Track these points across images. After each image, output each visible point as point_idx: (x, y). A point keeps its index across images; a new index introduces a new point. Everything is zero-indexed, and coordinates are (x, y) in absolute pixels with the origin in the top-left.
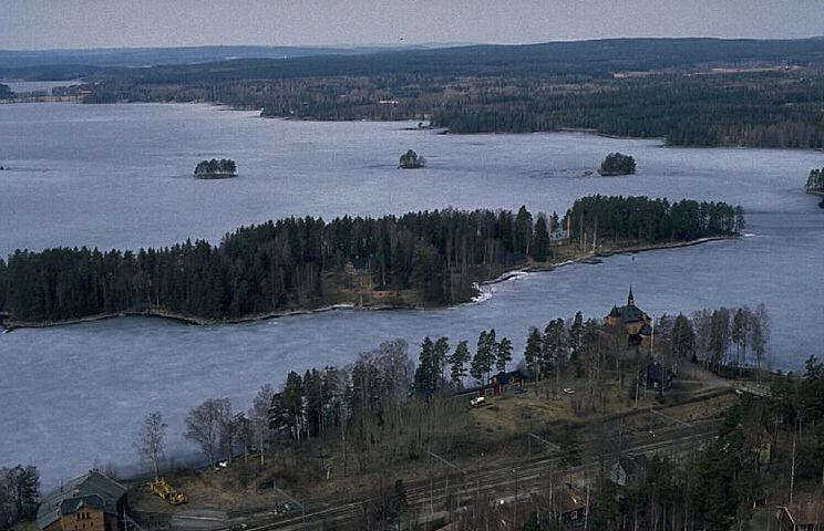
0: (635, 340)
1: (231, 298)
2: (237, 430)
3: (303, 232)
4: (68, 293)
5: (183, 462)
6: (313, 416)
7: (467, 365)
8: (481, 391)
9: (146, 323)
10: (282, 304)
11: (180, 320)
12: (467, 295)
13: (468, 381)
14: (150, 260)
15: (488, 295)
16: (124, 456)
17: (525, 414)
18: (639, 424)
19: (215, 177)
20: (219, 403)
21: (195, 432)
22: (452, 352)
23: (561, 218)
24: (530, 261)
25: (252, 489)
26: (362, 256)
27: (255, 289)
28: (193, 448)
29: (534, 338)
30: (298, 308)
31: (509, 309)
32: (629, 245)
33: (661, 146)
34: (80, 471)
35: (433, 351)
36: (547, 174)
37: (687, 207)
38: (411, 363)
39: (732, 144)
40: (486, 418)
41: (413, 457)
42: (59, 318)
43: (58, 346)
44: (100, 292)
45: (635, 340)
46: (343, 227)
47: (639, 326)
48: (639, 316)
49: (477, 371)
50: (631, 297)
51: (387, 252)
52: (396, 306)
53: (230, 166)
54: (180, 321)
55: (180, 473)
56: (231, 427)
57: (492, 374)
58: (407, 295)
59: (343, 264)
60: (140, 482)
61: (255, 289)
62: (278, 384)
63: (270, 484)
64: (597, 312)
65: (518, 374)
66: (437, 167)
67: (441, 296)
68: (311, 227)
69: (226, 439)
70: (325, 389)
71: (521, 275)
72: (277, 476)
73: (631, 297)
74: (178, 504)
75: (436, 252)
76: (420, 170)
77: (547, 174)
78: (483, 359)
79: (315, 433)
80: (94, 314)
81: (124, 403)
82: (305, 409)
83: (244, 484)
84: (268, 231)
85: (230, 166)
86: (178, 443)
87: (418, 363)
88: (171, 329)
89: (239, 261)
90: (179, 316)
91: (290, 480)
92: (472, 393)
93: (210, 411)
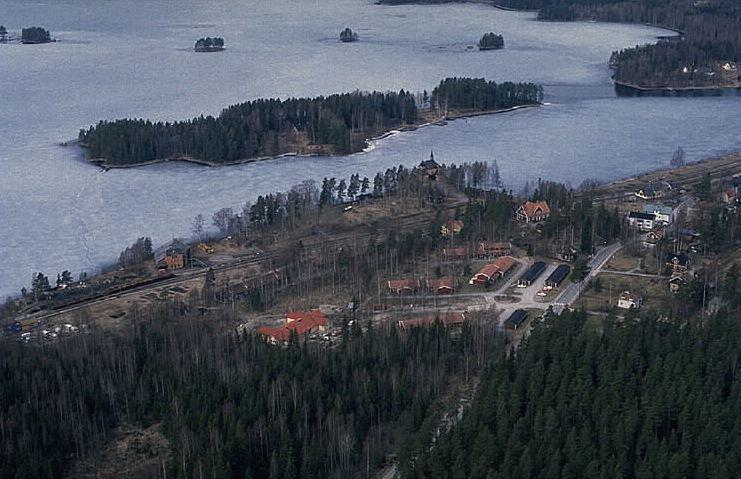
0: (432, 177)
1: (228, 151)
2: (235, 221)
3: (267, 107)
4: (136, 150)
5: (212, 237)
6: (270, 216)
7: (346, 191)
8: (351, 203)
9: (180, 164)
10: (256, 154)
11: (199, 163)
12: (361, 147)
13: (346, 199)
14: (181, 127)
15: (373, 147)
16: (186, 234)
17: (369, 214)
18: (421, 219)
19: (209, 50)
20: (228, 210)
21: (217, 223)
22: (337, 185)
23: (429, 94)
24: (404, 124)
25: (242, 247)
26: (301, 123)
27: (240, 146)
28: (215, 230)
29: (378, 178)
30: (265, 155)
31: (385, 154)
32: (470, 111)
33: (534, 20)
34: (169, 240)
35: (328, 185)
36: (441, 48)
37: (508, 86)
38: (318, 191)
39: (586, 18)
40: (350, 216)
41: (314, 234)
42: (132, 162)
43: (136, 179)
44: (154, 148)
45: (432, 177)
46: (292, 104)
47: (435, 170)
48: (435, 165)
49: (350, 194)
50: (432, 156)
51: (316, 122)
52: (320, 154)
53: (220, 42)
54: (199, 163)
55: (211, 241)
56: (232, 221)
57: (358, 194)
58: (327, 148)
59: (291, 127)
60: (194, 244)
61: (240, 146)
62: (254, 201)
63: (250, 245)
64: (412, 164)
65: (369, 195)
66: (368, 40)
67: (345, 148)
68: (273, 104)
69: (230, 226)
70: (276, 203)
71: (396, 132)
72: (254, 241)
73: (432, 156)
74: (211, 253)
75: (343, 123)
76: (352, 44)
77: (441, 48)
78: (353, 187)
79: (270, 223)
80: (152, 160)
81: (466, 178)
82: (267, 212)
83: (239, 245)
84: (248, 107)
85: (220, 42)
86: (210, 228)
87: (321, 190)
88: (195, 169)
89: (231, 130)
90: (199, 161)
91: (259, 243)
92: (347, 204)
93: (222, 215)
